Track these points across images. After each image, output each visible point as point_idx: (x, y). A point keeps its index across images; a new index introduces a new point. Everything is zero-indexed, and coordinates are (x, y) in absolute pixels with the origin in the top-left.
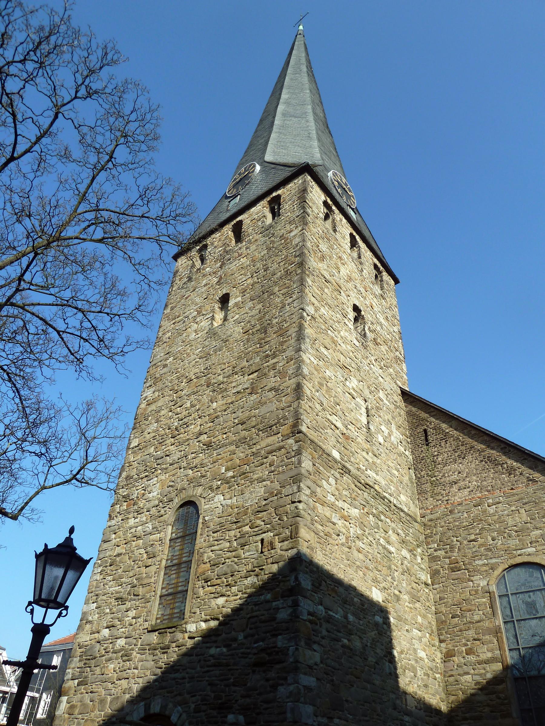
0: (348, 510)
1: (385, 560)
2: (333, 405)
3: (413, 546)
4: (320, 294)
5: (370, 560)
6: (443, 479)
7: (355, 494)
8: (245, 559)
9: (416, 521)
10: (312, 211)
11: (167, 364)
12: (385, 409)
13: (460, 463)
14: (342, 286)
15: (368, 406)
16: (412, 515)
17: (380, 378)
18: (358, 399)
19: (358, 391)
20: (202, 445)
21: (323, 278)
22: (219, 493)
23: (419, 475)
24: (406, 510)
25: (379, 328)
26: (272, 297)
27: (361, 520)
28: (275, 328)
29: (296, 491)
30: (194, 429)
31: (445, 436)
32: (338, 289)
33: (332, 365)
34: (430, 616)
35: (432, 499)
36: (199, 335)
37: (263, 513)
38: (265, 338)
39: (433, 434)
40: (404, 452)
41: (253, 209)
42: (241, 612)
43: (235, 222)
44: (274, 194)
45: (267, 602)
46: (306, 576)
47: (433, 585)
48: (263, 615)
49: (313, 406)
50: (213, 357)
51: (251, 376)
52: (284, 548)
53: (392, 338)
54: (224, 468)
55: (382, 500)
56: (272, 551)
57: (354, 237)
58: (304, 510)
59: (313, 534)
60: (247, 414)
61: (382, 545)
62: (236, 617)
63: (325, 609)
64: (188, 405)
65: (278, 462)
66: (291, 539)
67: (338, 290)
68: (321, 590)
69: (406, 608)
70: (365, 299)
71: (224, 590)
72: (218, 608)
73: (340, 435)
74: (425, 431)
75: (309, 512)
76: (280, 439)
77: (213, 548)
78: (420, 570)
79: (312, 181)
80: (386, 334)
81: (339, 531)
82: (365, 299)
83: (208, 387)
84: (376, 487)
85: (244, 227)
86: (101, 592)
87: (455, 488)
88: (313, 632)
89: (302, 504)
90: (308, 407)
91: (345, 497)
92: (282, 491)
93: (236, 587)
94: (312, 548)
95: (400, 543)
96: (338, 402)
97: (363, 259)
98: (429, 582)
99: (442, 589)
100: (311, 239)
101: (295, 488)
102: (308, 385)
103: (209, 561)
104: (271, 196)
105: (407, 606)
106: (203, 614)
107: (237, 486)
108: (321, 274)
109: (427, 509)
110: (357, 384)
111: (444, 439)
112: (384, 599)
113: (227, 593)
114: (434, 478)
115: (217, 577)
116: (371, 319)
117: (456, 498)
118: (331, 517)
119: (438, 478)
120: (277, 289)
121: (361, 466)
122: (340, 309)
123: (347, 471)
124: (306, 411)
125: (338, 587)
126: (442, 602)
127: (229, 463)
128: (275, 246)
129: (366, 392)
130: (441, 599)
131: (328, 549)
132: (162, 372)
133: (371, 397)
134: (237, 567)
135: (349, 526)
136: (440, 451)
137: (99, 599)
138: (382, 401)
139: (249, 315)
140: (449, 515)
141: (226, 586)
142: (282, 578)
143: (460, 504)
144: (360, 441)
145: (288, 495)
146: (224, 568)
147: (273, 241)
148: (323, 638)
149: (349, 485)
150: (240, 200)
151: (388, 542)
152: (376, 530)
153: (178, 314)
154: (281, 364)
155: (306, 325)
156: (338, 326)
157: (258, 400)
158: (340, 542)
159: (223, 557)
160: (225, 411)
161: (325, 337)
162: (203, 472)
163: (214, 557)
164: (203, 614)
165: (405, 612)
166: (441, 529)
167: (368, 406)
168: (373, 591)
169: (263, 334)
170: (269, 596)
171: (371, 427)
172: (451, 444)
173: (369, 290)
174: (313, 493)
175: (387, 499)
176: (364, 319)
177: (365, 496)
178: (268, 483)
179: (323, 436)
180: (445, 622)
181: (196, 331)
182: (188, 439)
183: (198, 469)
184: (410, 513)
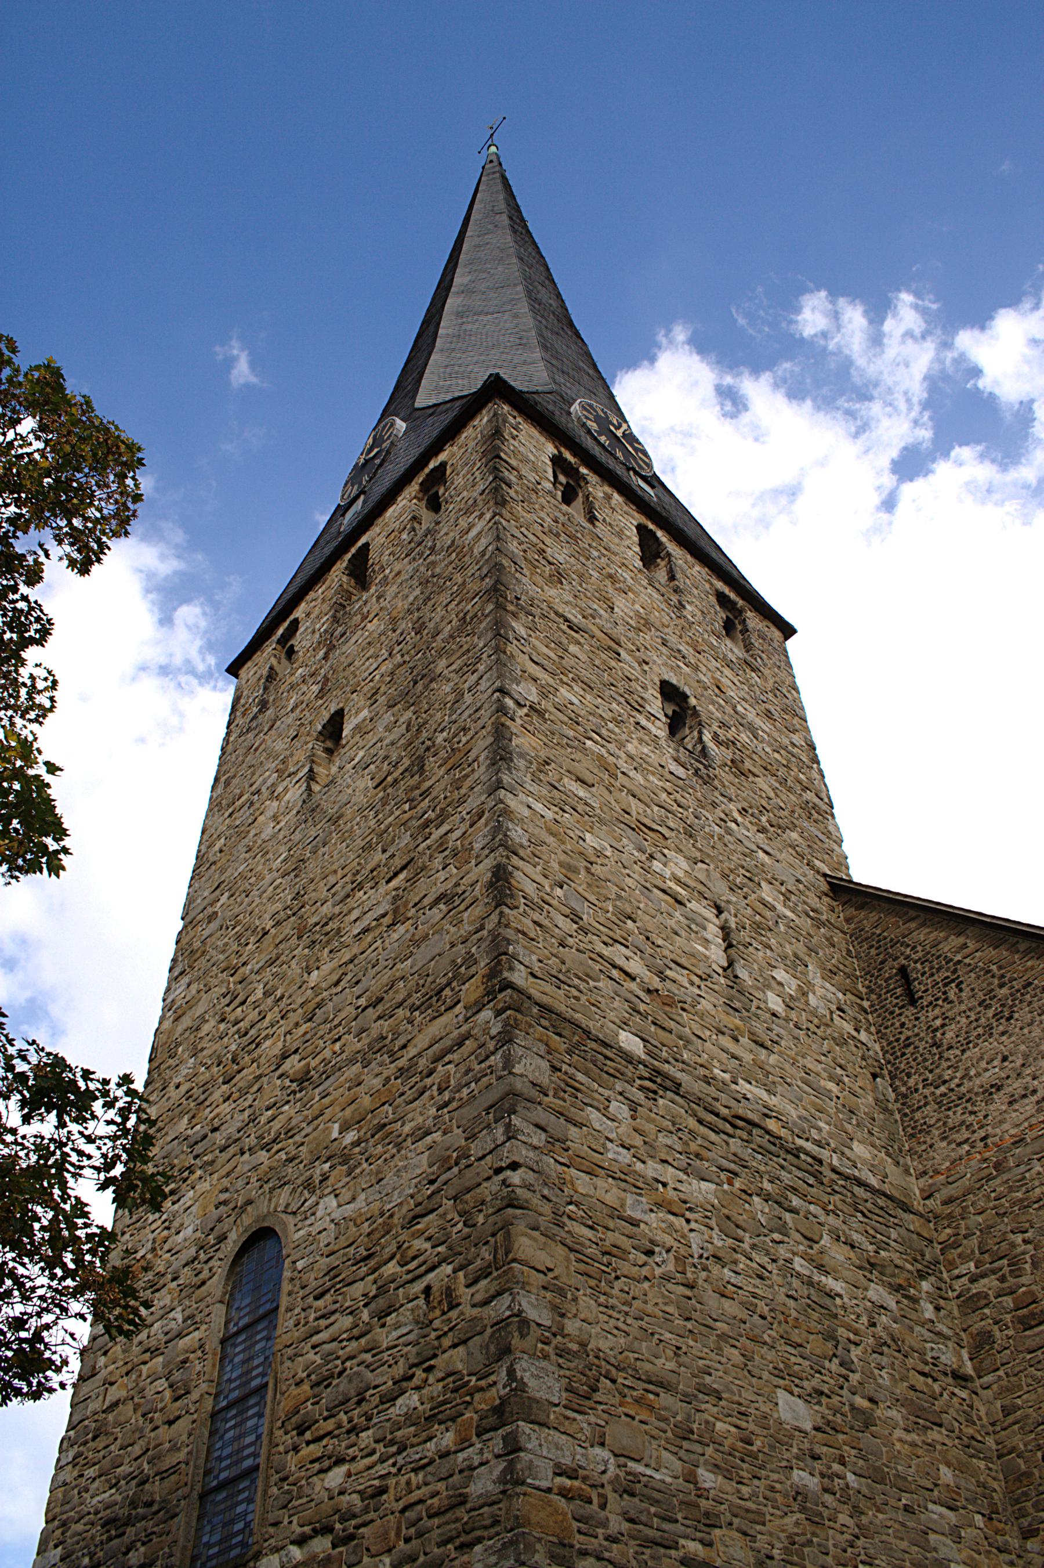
0: (678, 1185)
1: (815, 1316)
2: (614, 919)
3: (906, 1275)
4: (556, 658)
5: (763, 1317)
6: (967, 1085)
7: (699, 1141)
8: (388, 1349)
9: (907, 1209)
10: (520, 477)
11: (216, 913)
12: (782, 928)
13: (1003, 1034)
14: (623, 639)
15: (726, 921)
16: (896, 1194)
17: (761, 854)
18: (693, 905)
19: (692, 884)
20: (287, 1083)
21: (561, 620)
22: (326, 1191)
23: (903, 1089)
24: (873, 1181)
25: (744, 737)
26: (434, 685)
27: (726, 1211)
28: (443, 754)
29: (501, 1139)
30: (271, 1048)
31: (954, 972)
32: (613, 647)
33: (601, 821)
34: (982, 1464)
35: (944, 1144)
36: (282, 824)
37: (426, 1219)
38: (420, 783)
39: (923, 975)
40: (855, 1034)
41: (391, 510)
42: (385, 1497)
43: (353, 550)
44: (432, 465)
45: (444, 1455)
46: (544, 1364)
47: (980, 1377)
48: (435, 1494)
49: (546, 922)
50: (311, 865)
51: (394, 883)
52: (479, 1298)
53: (789, 761)
54: (336, 1126)
55: (789, 1157)
56: (453, 1314)
57: (652, 533)
58: (529, 1187)
59: (561, 1251)
60: (385, 978)
61: (799, 1275)
62: (372, 1515)
63: (616, 1455)
64: (259, 993)
65: (458, 1075)
66: (497, 1269)
67: (610, 648)
68: (600, 1403)
69: (898, 1446)
70: (696, 669)
71: (343, 1444)
72: (331, 1498)
73: (642, 994)
74: (903, 971)
75: (546, 1192)
76: (461, 1017)
77: (316, 1339)
78: (935, 1338)
79: (515, 413)
80: (768, 749)
81: (652, 1242)
82: (696, 669)
83: (300, 938)
84: (772, 1125)
85: (374, 556)
86: (72, 1514)
87: (1000, 1101)
88: (575, 1525)
89: (520, 1171)
90: (531, 925)
91: (664, 1150)
92: (469, 1149)
93: (370, 1432)
94: (561, 1289)
95: (860, 1268)
96: (629, 910)
97: (681, 581)
98: (969, 1369)
99: (1004, 1383)
100: (520, 536)
101: (499, 1132)
102: (528, 869)
103: (309, 1376)
104: (427, 471)
105: (900, 1440)
106: (295, 1522)
107: (365, 1165)
108: (556, 613)
109: (937, 1172)
110: (688, 869)
111: (953, 981)
112: (820, 1422)
113: (350, 1451)
114: (943, 1089)
115: (326, 1414)
116: (718, 715)
117: (1005, 1126)
118: (623, 1205)
119: (953, 1086)
120: (443, 663)
121: (716, 1071)
122: (621, 691)
123: (668, 1083)
124: (524, 934)
125: (657, 1395)
126: (1011, 1419)
127: (348, 1111)
128: (438, 570)
129: (720, 888)
130: (1007, 1411)
131: (615, 1292)
132: (206, 933)
133: (734, 899)
134: (369, 1374)
135: (686, 1227)
136: (949, 1014)
137: (68, 1534)
138: (772, 909)
139: (387, 741)
140: (994, 1178)
141: (349, 1432)
142: (478, 1380)
143: (1019, 1141)
144: (710, 1007)
145: (484, 1156)
146: (342, 1386)
147: (433, 563)
148: (612, 1539)
149: (678, 1120)
150: (364, 502)
151: (821, 1268)
152: (776, 1236)
153: (238, 791)
154: (457, 834)
155: (515, 727)
156: (617, 730)
157: (408, 936)
158: (658, 1271)
159: (338, 1358)
160: (337, 984)
161: (578, 756)
162: (292, 1148)
163: (319, 1361)
164: (295, 1522)
165: (896, 1457)
166: (980, 1219)
167: (726, 921)
168: (780, 1402)
169: (417, 777)
170: (448, 1439)
171: (743, 974)
172: (973, 990)
173: (706, 648)
174: (557, 1142)
175: (807, 1154)
176: (699, 716)
177: (733, 1149)
178: (437, 1136)
179: (583, 998)
180: (1028, 1474)
181: (275, 818)
182: (260, 1076)
183: (280, 1146)
184: (886, 1188)
